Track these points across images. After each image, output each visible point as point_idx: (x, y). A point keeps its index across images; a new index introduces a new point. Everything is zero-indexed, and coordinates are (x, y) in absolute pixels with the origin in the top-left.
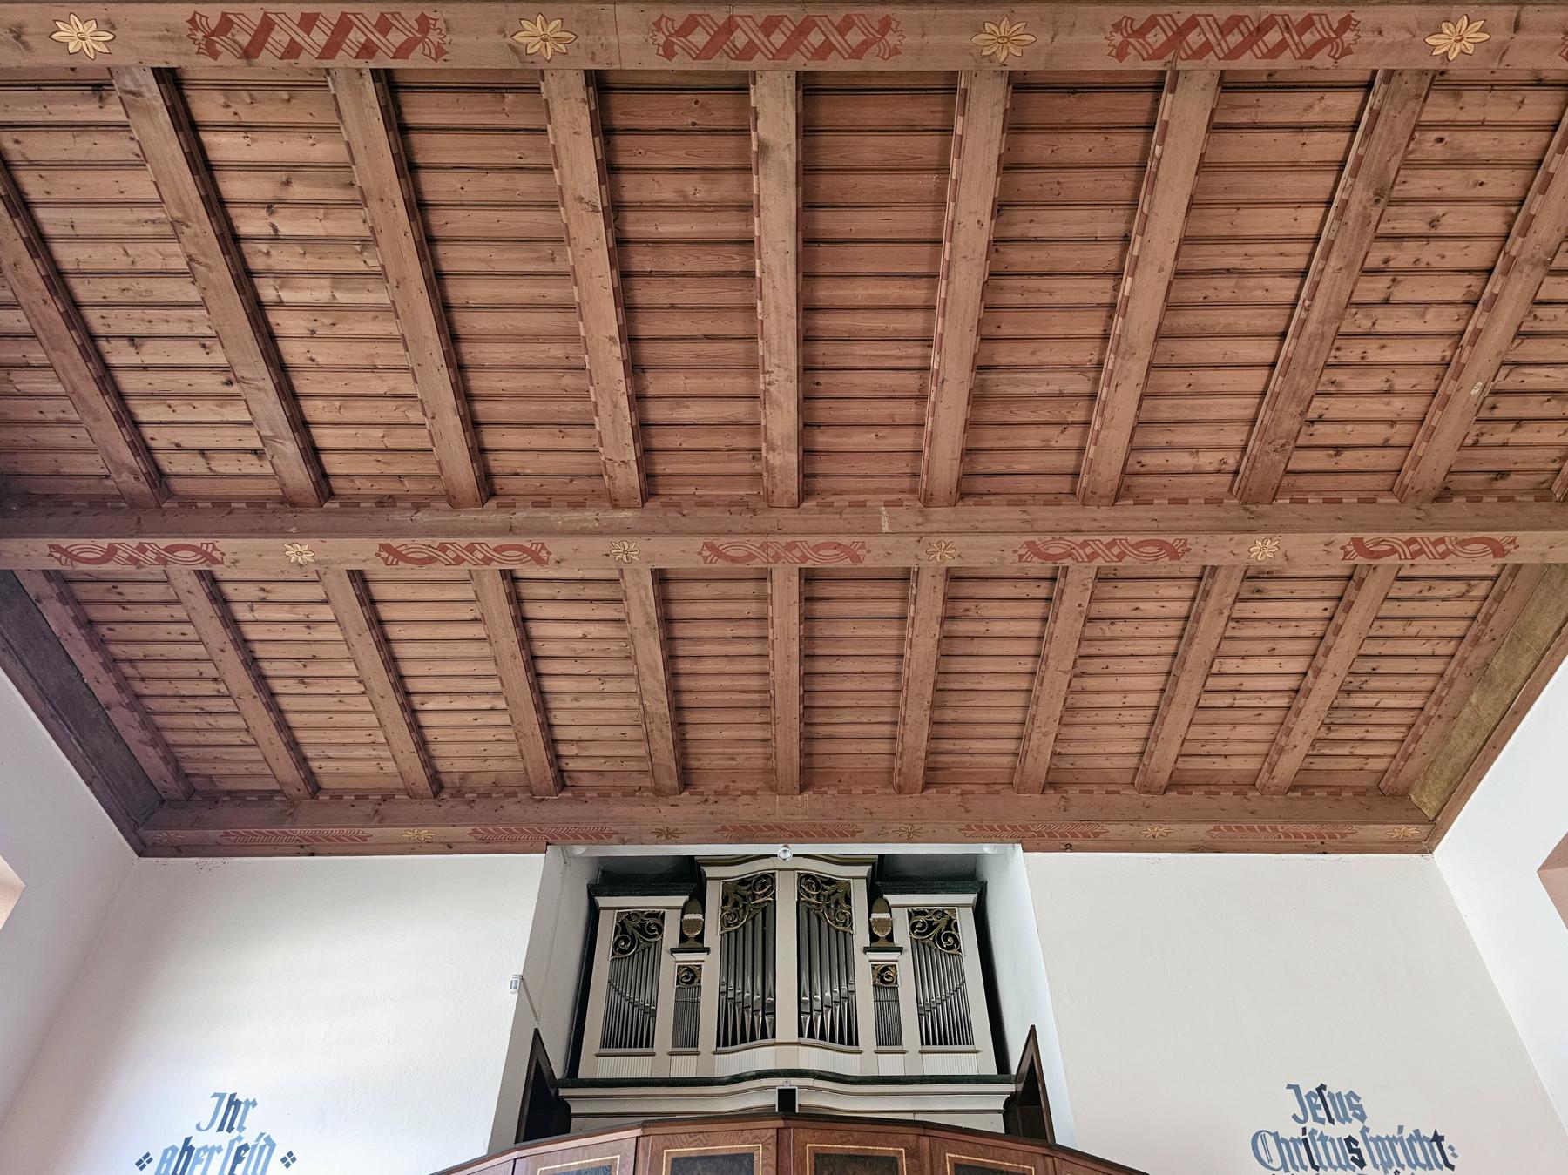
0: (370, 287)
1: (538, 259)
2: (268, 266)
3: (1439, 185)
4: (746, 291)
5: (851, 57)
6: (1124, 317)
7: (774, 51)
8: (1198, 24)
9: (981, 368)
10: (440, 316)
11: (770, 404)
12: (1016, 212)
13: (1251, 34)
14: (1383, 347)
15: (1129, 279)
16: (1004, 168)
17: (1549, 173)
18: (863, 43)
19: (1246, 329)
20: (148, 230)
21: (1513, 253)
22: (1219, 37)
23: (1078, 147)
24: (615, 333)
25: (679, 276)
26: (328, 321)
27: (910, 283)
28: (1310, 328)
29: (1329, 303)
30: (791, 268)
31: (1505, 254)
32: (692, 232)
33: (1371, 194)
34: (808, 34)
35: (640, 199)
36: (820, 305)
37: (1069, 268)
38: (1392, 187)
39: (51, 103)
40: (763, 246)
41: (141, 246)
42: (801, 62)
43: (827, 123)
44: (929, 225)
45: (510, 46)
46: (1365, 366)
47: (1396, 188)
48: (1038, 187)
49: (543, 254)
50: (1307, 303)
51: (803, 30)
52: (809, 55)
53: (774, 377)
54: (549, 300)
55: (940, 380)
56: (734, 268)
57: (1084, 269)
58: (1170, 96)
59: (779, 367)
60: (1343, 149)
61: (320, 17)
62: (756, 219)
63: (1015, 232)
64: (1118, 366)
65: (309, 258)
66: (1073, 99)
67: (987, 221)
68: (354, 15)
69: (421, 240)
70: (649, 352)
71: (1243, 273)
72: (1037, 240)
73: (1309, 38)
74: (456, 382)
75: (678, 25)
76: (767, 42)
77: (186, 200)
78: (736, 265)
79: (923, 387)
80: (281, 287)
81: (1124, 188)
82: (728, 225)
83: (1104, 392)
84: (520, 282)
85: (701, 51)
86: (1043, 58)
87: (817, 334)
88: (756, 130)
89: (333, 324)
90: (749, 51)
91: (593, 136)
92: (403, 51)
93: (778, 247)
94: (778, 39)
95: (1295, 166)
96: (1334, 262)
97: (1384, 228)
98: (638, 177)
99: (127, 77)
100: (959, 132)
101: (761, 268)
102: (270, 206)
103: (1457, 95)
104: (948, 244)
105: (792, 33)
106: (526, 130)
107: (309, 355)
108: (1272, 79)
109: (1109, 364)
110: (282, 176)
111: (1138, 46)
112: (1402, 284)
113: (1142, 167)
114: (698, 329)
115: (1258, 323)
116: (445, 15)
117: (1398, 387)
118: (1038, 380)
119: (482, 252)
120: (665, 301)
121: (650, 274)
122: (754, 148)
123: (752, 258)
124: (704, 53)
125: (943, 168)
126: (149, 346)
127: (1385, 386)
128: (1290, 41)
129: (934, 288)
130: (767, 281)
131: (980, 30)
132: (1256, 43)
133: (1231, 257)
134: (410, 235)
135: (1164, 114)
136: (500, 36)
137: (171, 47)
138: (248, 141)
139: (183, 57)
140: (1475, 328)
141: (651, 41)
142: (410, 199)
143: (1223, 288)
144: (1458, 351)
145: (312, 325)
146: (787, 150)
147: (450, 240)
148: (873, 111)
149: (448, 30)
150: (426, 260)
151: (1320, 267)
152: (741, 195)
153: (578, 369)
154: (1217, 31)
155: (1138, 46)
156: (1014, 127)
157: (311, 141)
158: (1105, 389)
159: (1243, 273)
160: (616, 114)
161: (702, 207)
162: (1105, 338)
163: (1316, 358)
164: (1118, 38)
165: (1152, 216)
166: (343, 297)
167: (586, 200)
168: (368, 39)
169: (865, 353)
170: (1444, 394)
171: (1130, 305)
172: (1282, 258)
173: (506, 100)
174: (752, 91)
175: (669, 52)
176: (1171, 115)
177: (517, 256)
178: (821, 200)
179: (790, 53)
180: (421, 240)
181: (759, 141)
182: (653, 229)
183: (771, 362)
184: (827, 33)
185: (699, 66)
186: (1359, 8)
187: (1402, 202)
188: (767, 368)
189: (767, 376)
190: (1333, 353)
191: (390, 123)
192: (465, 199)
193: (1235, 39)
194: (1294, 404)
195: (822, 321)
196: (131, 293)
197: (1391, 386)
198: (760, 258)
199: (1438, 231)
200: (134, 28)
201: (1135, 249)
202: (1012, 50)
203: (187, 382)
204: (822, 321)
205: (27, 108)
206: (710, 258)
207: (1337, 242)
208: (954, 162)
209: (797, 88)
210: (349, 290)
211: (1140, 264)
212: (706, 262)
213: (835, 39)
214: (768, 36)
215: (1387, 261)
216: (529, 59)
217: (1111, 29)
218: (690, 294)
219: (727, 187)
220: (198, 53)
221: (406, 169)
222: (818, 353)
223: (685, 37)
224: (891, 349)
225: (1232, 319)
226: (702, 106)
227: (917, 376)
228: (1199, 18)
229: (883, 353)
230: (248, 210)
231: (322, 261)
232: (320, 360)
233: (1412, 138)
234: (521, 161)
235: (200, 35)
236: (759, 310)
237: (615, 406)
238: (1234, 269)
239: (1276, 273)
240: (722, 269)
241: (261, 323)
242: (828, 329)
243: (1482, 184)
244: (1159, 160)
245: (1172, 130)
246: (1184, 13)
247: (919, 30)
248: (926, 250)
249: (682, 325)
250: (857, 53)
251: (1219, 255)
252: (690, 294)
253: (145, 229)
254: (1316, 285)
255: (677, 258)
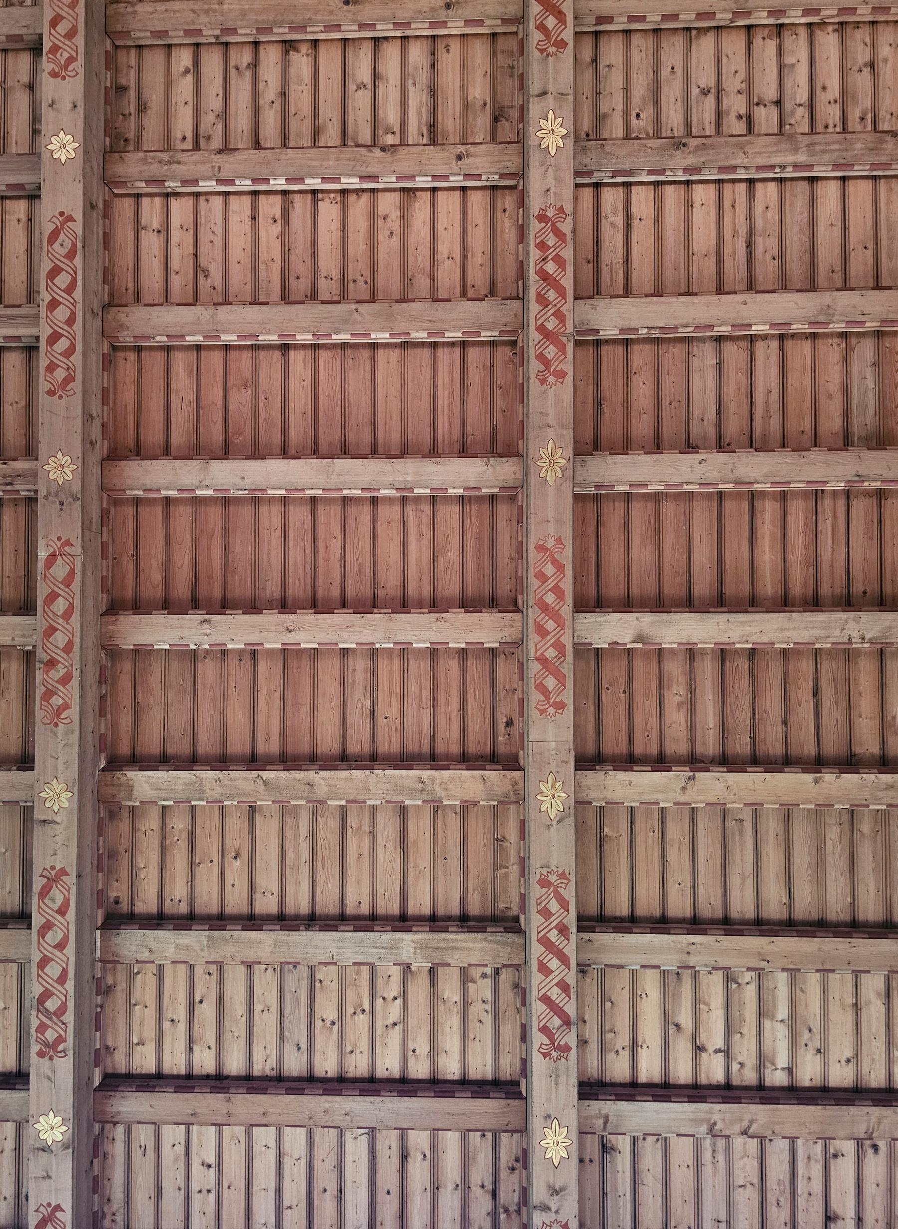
0: (772, 986)
1: (741, 833)
2: (753, 1069)
3: (674, 100)
4: (768, 657)
5: (563, 572)
6: (790, 324)
7: (559, 628)
8: (542, 324)
9: (846, 441)
10: (797, 931)
11: (886, 637)
12: (695, 432)
13: (548, 284)
14: (824, 88)
15: (754, 327)
16: (658, 448)
17: (662, 20)
18: (553, 564)
19: (806, 215)
20: (721, 1157)
21: (730, 16)
22: (550, 306)
23: (642, 392)
24: (809, 777)
25: (754, 714)
26: (806, 1035)
27: (758, 515)
28: (802, 158)
29: (777, 151)
30: (742, 617)
31: (732, 23)
32: (714, 699)
33: (678, 152)
34: (547, 604)
35: (685, 740)
36: (780, 592)
37: (744, 380)
38: (673, 137)
39: (616, 1190)
40: (723, 640)
41: (737, 1172)
42: (566, 610)
43: (621, 587)
44: (706, 503)
45: (558, 822)
46: (845, 97)
47: (676, 134)
48: (674, 419)
49: (736, 828)
50: (777, 170)
51: (545, 608)
52: (562, 603)
53: (855, 634)
54: (780, 830)
55: (857, 478)
56: (747, 665)
57: (745, 368)
58: (601, 332)
59: (844, 629)
60: (644, 188)
61: (541, 959)
62: (699, 646)
63: (712, 433)
64: (842, 318)
65: (745, 1030)
66: (605, 405)
67: (699, 456)
68: (539, 933)
69: (725, 930)
70: (832, 746)
71: (751, 233)
72: (719, 412)
73: (551, 241)
74: (868, 933)
75: (542, 698)
76: (553, 634)
77: (692, 1116)
78: (744, 664)
79: (867, 494)
80: (773, 1064)
81: (676, 351)
82: (707, 670)
83: (871, 325)
84: (764, 853)
85: (560, 682)
86: (564, 432)
87: (811, 592)
88: (626, 644)
89: (810, 1030)
90: (559, 647)
91: (632, 771)
92: (564, 904)
93: (723, 629)
94: (551, 625)
95: (658, 221)
96: (739, 160)
97: (710, 130)
98: (667, 740)
99: (594, 1121)
100: (627, 488)
101: (743, 643)
102: (699, 1049)
103: (605, 116)
104: (720, 486)
105: (547, 615)
106: (631, 823)
107: (843, 1063)
108: (591, 260)
109: (840, 327)
110: (672, 1029)
111: (557, 363)
112: (762, 95)
113: (657, 341)
114: (808, 702)
115: (799, 204)
116: (538, 866)
117: (867, 58)
118: (859, 389)
119: (735, 881)
120: (779, 729)
121: (753, 739)
122: (640, 646)
123: (737, 650)
124: (561, 679)
125: (658, 497)
126: (835, 1205)
127: (866, 71)
128: (553, 254)
129: (763, 494)
130: (757, 638)
131: (545, 479)
132: (554, 279)
133: (736, 249)
134: (719, 938)
135: (614, 334)
136: (552, 829)
137: (563, 1079)
138: (644, 1046)
139: (570, 1073)
140: (803, 16)
141: (553, 718)
142: (688, 929)
143: (765, 245)
144: (827, 21)
145: (811, 1051)
146: (642, 620)
147: (790, 906)
148: (614, 557)
149: (548, 867)
150: (742, 930)
151: (743, 171)
152: (681, 657)
153: (852, 816)
154: (546, 309)
155: (557, 363)
156: (625, 446)
157: (644, 996)
158: (867, 324)
159: (751, 233)
160: (617, 751)
161: (692, 690)
162: (814, 336)
163: (833, 143)
164: (551, 379)
165: (696, 322)
166: (782, 1012)
167: (684, 784)
168: (555, 927)
169: (830, 550)
170: (871, 14)
171: (779, 321)
172: (737, 205)
173: (609, 834)
174: (597, 646)
175: (560, 706)
176: (615, 328)
177: (738, 851)
178: (684, 592)
179: (560, 616)
180: (725, 930)
181: (634, 642)
182: (712, 732)
183: (837, 636)
184: (546, 590)
185: (570, 683)
186: (532, 211)
187: (688, 124)
188: (845, 640)
189: (853, 640)
190: (831, 129)
191: (626, 928)
192: (688, 883)
193: (552, 295)
194: (884, 146)
195: (797, 589)
196: (781, 1199)
197: (865, 65)
198: (734, 643)
199: (713, 85)
200: (549, 1100)
201: (726, 329)
202: (558, 456)
203: (874, 1186)
204: (797, 589)
205: (621, 1210)
206: (737, 686)
207: (720, 164)
208: (651, 488)
209: (594, 612)
210: (775, 1006)
211: (739, 322)
212: (741, 687)
213: (551, 584)
214: (548, 633)
215: (740, 117)
216: (567, 810)
217: (545, 386)
218: (772, 703)
219: (675, 669)
220: (566, 1059)
221: (694, 926)
222: (830, 594)
223: (550, 693)
224: (826, 527)
225: (796, 229)
226: (611, 685)
227: (855, 501)
228: (538, 324)
229: (829, 534)
230: (703, 1068)
231: (747, 1019)
232: (849, 1053)
233: (637, 138)
234: (656, 831)
235: (554, 1053)
236: (785, 646)
237: (892, 787)
238: (747, 242)
239: (750, 206)
240: (747, 676)
241: (809, 1094)
242: (805, 585)
243: (673, 68)
244: (650, 328)
245: (626, 324)
246: (534, 335)
247: (544, 524)
248: (728, 505)
249: (804, 714)
250: (560, 567)
251: (734, 259)
252: (772, 703)
253: (720, 1160)
254: (760, 168)
255: (737, 715)
